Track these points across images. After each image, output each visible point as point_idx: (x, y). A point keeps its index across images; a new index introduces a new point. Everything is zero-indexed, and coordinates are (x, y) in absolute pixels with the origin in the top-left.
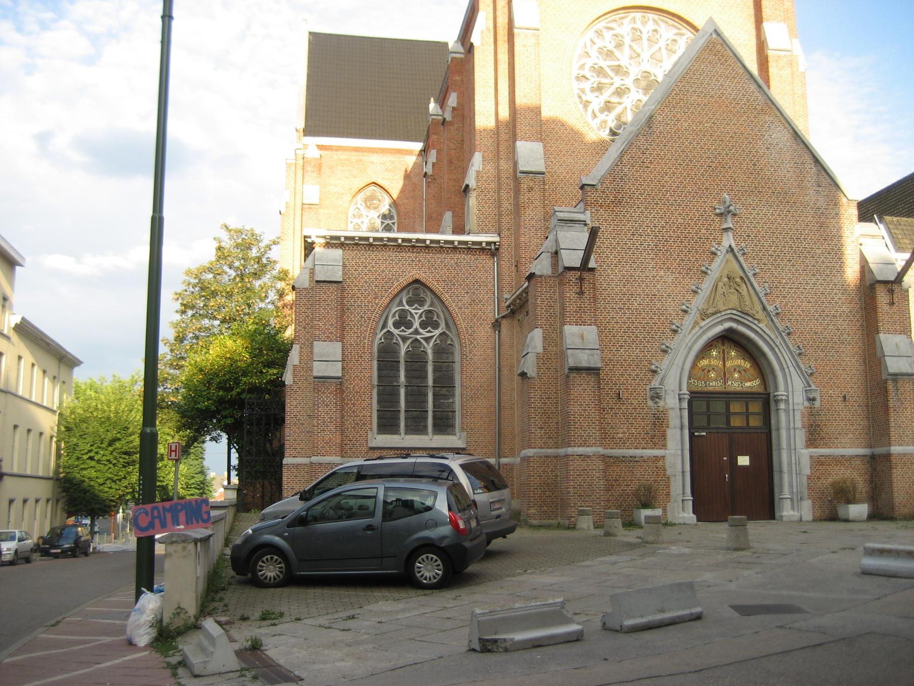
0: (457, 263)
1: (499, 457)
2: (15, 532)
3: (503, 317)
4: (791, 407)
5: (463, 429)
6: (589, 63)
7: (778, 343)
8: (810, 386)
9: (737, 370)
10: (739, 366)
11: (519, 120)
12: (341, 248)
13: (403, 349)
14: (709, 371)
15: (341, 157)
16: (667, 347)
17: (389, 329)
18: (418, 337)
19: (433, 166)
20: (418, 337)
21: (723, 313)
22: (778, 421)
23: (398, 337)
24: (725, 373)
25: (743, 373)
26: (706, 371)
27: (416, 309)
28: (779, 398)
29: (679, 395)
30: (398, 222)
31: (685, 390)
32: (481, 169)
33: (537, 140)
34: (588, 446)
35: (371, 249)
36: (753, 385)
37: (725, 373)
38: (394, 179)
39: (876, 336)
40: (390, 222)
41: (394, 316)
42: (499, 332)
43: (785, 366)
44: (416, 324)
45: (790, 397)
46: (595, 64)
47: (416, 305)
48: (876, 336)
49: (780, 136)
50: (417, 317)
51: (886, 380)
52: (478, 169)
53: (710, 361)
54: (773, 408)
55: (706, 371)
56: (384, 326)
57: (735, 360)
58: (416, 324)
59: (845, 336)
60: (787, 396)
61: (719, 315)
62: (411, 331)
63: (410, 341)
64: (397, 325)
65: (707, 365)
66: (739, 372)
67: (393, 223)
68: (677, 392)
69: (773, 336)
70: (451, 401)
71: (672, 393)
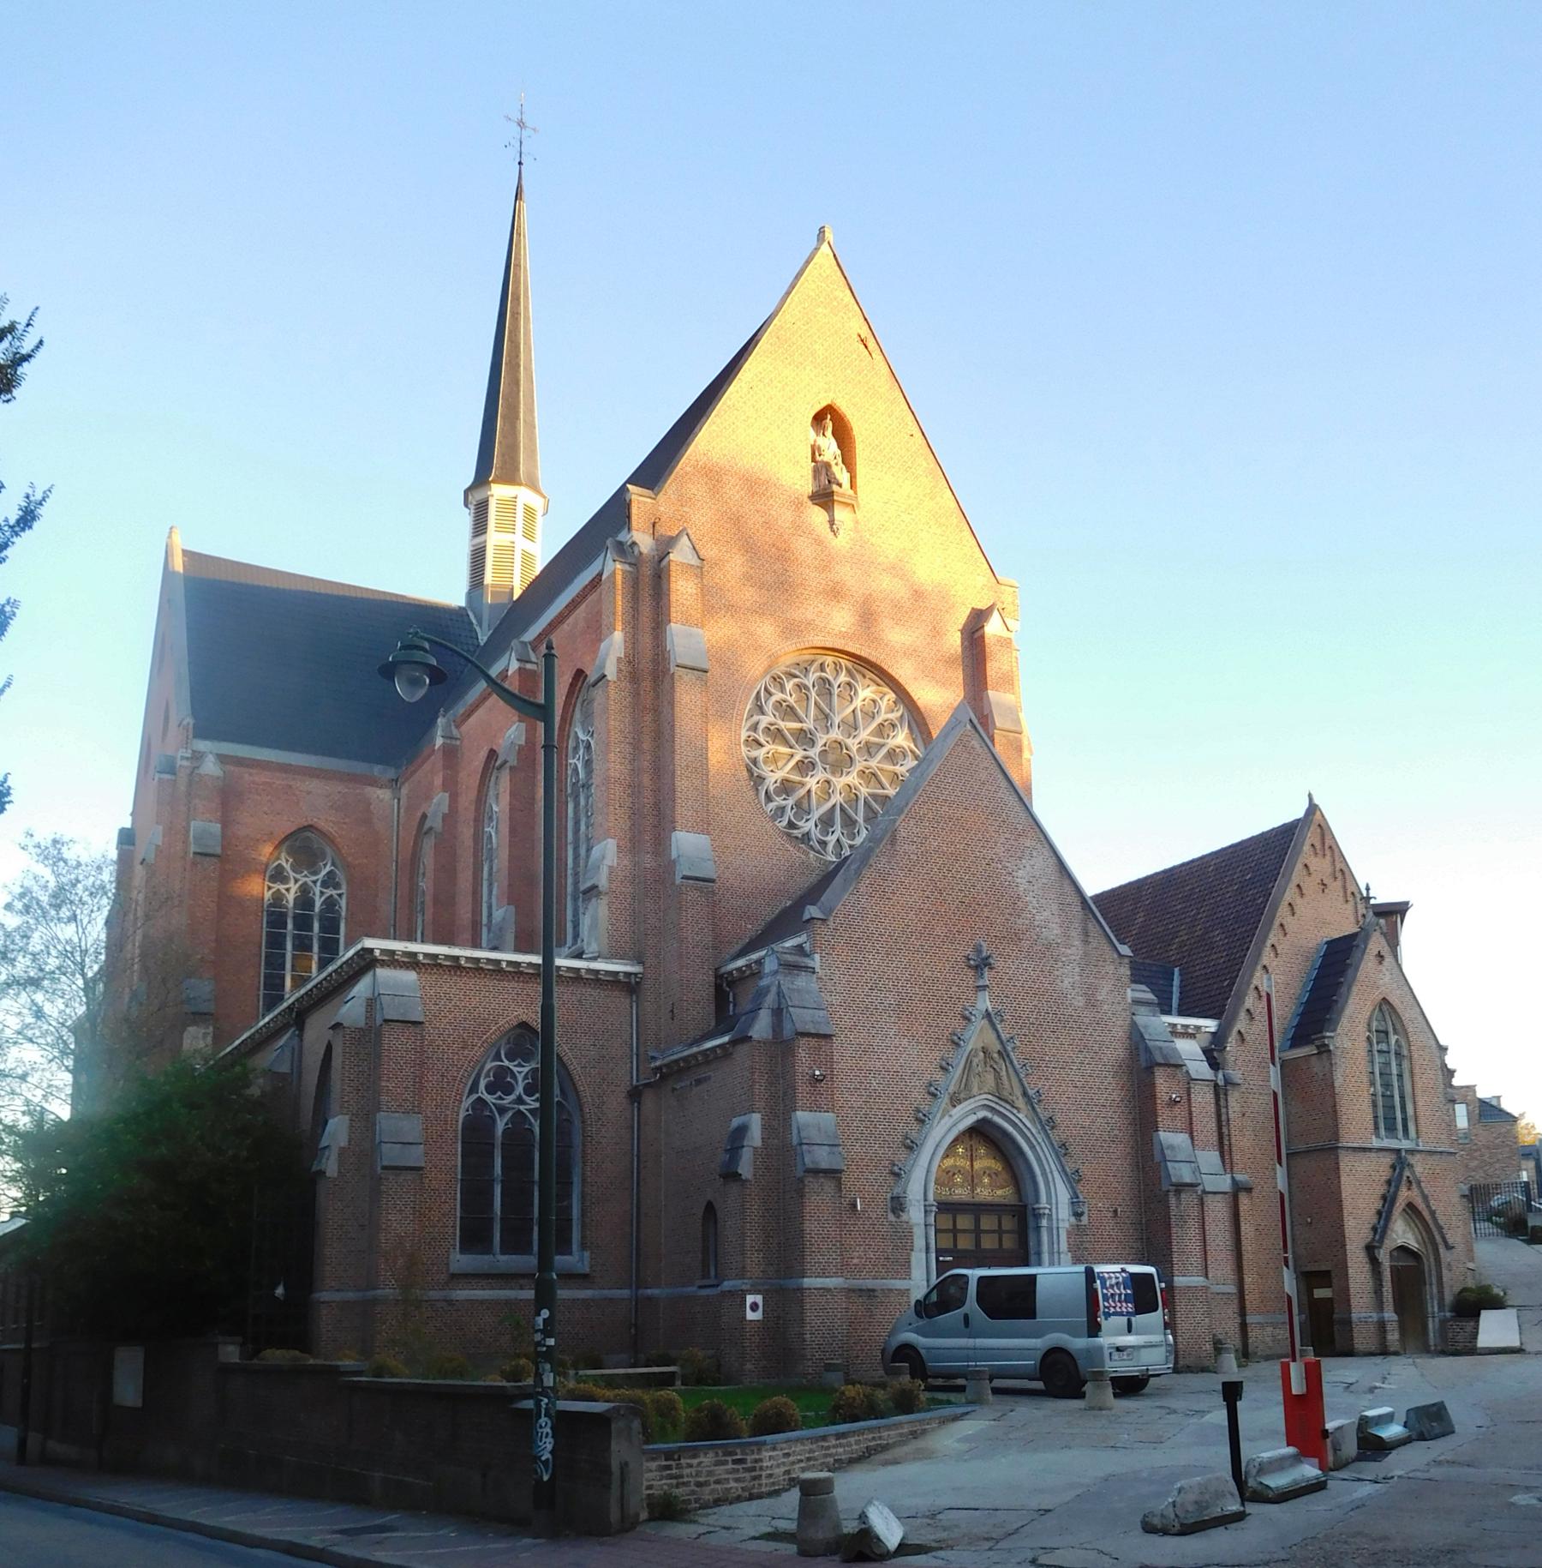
0: (579, 1001)
1: (638, 1288)
2: (1315, 1356)
3: (646, 1085)
4: (1055, 1225)
5: (583, 1246)
6: (765, 721)
7: (1040, 1140)
8: (1078, 1197)
9: (988, 1172)
10: (989, 1168)
11: (679, 801)
12: (414, 969)
13: (501, 1125)
14: (954, 1174)
15: (256, 779)
16: (912, 1142)
17: (480, 1094)
18: (522, 1108)
19: (443, 820)
20: (522, 1108)
21: (977, 1098)
22: (1039, 1243)
23: (493, 1107)
24: (973, 1176)
25: (994, 1176)
26: (951, 1174)
27: (519, 1065)
28: (1041, 1211)
29: (925, 1206)
30: (348, 894)
31: (931, 1197)
32: (615, 865)
33: (702, 832)
34: (827, 1277)
35: (458, 973)
36: (1003, 1194)
37: (973, 1176)
38: (345, 823)
39: (1155, 1134)
40: (334, 892)
41: (487, 1075)
42: (639, 1103)
43: (1048, 1170)
44: (519, 1090)
45: (1054, 1210)
46: (772, 725)
47: (520, 1060)
48: (1155, 1134)
49: (1039, 863)
50: (520, 1078)
51: (1168, 1191)
52: (610, 864)
53: (955, 1160)
54: (1031, 1223)
55: (951, 1174)
56: (474, 1088)
57: (985, 1162)
58: (519, 1090)
59: (1116, 1132)
60: (1050, 1210)
61: (972, 1100)
62: (512, 1097)
63: (510, 1114)
64: (491, 1089)
65: (952, 1166)
66: (989, 1175)
67: (340, 895)
68: (922, 1203)
69: (1034, 1131)
70: (565, 1203)
71: (917, 1204)
